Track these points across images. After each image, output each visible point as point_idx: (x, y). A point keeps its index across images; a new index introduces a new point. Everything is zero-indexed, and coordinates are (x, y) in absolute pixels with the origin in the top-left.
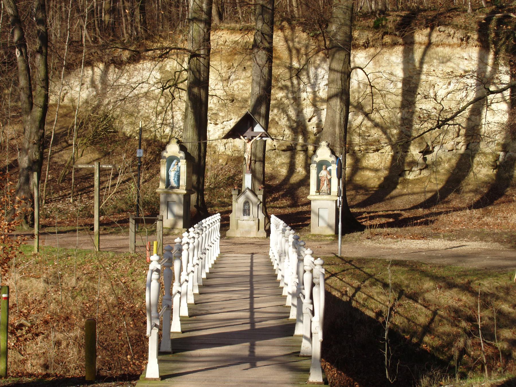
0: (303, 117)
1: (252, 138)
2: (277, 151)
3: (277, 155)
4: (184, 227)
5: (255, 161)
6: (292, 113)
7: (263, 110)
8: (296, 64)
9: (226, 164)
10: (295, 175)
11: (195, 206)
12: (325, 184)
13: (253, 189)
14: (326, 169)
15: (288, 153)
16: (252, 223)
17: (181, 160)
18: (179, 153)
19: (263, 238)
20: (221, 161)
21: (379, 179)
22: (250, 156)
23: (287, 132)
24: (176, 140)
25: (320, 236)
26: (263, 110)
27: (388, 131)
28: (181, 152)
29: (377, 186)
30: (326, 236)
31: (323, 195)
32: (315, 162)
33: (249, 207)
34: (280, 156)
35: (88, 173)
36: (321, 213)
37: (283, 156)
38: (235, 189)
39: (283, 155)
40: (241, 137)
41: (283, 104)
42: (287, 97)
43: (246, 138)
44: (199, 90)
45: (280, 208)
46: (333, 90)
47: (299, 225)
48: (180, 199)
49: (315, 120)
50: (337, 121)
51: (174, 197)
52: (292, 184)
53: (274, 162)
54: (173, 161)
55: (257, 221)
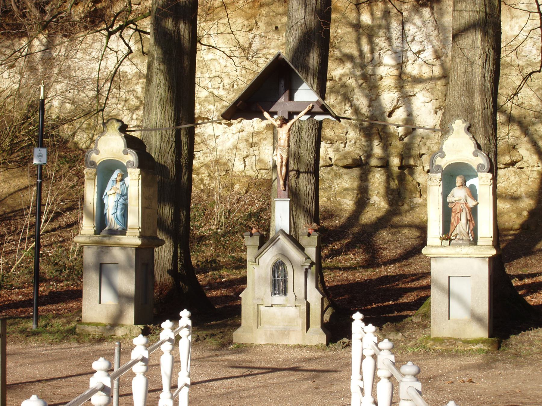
0: (380, 106)
1: (291, 115)
2: (334, 167)
3: (335, 175)
4: (136, 323)
5: (298, 173)
6: (362, 102)
7: (314, 60)
8: (366, 18)
9: (247, 192)
10: (368, 209)
11: (169, 272)
12: (463, 220)
13: (293, 234)
14: (464, 184)
15: (356, 172)
16: (293, 312)
17: (129, 170)
18: (125, 153)
19: (318, 348)
20: (237, 187)
21: (519, 214)
22: (285, 156)
23: (353, 134)
24: (117, 125)
25: (453, 341)
26: (314, 60)
27: (532, 129)
28: (129, 150)
29: (517, 226)
30: (468, 342)
31: (460, 245)
32: (439, 166)
33: (286, 275)
34: (340, 176)
35: (8, 210)
36: (456, 286)
37: (345, 177)
38: (251, 235)
39: (346, 174)
40: (266, 114)
41: (344, 86)
42: (352, 75)
43: (276, 117)
44: (176, 24)
45: (346, 269)
46: (466, 15)
47: (391, 309)
48: (129, 258)
49: (400, 115)
50: (477, 81)
51: (118, 255)
52: (366, 225)
53: (330, 187)
54: (112, 172)
55: (304, 308)
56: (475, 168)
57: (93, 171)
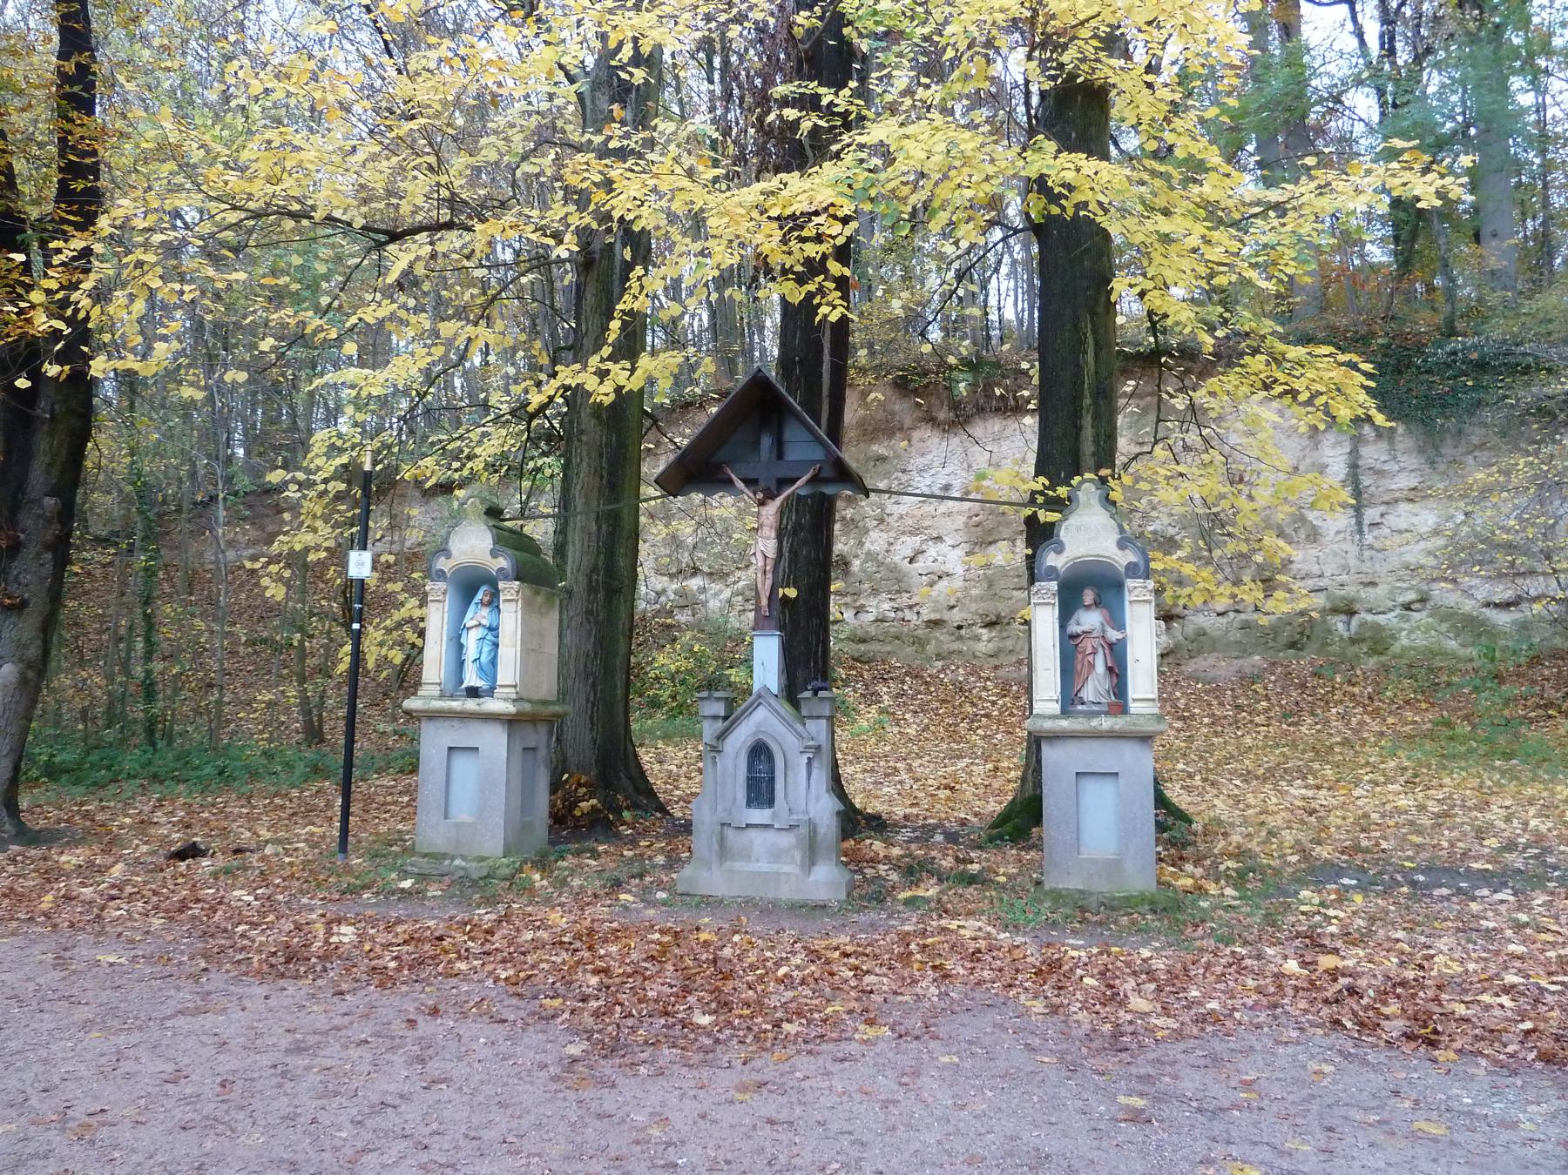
17: (501, 585)
18: (494, 554)
32: (1053, 568)
33: (772, 771)
56: (1122, 570)
57: (442, 585)
